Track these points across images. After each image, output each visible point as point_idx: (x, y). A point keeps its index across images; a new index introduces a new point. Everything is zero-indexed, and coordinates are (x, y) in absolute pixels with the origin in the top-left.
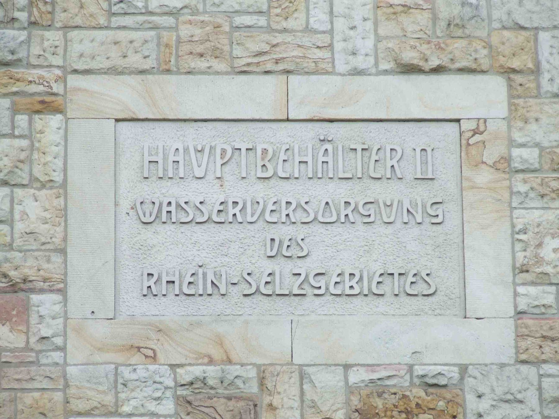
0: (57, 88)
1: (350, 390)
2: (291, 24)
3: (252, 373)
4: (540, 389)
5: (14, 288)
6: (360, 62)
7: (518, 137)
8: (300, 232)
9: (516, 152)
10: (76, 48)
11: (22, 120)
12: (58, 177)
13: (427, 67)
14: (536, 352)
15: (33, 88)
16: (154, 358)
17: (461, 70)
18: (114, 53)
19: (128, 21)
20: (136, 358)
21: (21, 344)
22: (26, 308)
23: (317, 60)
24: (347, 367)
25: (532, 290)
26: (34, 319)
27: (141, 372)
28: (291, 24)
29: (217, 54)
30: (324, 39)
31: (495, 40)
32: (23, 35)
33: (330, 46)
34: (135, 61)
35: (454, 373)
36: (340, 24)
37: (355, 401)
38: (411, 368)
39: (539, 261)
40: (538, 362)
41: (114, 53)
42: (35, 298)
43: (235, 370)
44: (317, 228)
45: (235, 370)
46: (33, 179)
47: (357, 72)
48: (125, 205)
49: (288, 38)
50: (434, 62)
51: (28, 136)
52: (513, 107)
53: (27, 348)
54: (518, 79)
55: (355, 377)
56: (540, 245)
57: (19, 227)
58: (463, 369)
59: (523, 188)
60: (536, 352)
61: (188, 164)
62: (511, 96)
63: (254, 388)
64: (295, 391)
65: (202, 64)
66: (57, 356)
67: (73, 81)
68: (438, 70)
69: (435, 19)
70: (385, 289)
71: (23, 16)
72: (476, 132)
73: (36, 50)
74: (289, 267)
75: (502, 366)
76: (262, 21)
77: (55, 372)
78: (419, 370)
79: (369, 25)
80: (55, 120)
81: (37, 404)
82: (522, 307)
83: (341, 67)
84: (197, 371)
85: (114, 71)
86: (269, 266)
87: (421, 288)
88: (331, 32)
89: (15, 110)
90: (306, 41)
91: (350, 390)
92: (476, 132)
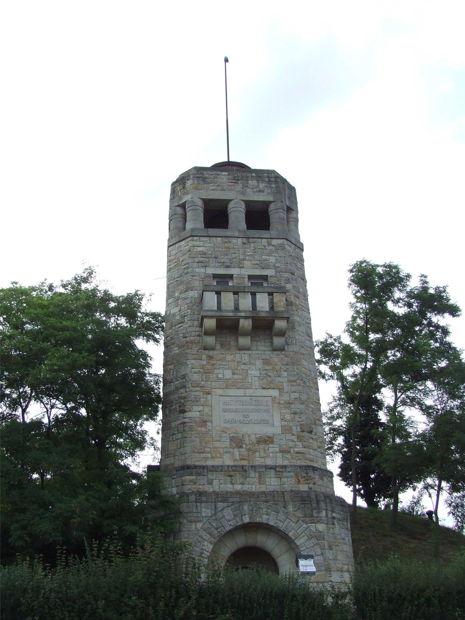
0: (210, 391)
1: (256, 438)
2: (246, 381)
3: (241, 435)
4: (285, 438)
5: (204, 422)
6: (257, 387)
7: (281, 399)
8: (248, 413)
9: (280, 401)
10: (213, 385)
11: (205, 396)
12: (211, 405)
13: (267, 388)
14: (284, 432)
15: (206, 391)
16: (226, 433)
17: (272, 389)
18: (219, 385)
19: (220, 380)
20: (223, 433)
21: (205, 430)
22: (206, 425)
23: (233, 387)
24: (256, 434)
25: (284, 422)
26: (207, 426)
27: (224, 435)
28: (246, 381)
29: (234, 386)
30: (250, 384)
31: (277, 384)
32: (205, 383)
33: (252, 385)
34: (222, 387)
35: (272, 435)
36: (253, 381)
37: (257, 440)
38: (266, 435)
39: (285, 418)
40: (285, 434)
41: (219, 385)
42: (207, 423)
43: (239, 435)
44: (250, 413)
45: (239, 435)
46: (207, 405)
47: (256, 389)
48: (221, 409)
49: (245, 383)
50: (268, 387)
51: (206, 398)
52: (280, 395)
53: (206, 431)
54: (281, 390)
55: (257, 436)
56: (285, 416)
57: (205, 412)
58: (274, 435)
59: (282, 407)
60: (284, 432)
61: (230, 403)
62: (279, 392)
63: (242, 438)
64: (248, 438)
65: (232, 387)
66: (211, 432)
67: (213, 390)
68: (268, 388)
69: (268, 381)
70: (261, 422)
71: (204, 380)
72: (275, 398)
73: (207, 385)
74: (246, 419)
75: (280, 434)
76: (241, 381)
77: (211, 435)
78: (267, 435)
79: (258, 382)
80: (210, 396)
81: (298, 398)
82: (282, 425)
83: (253, 388)
84: (233, 435)
85: (219, 388)
86: (244, 419)
87: (267, 422)
88: (252, 383)
89: (204, 394)
90: (248, 384)
91: (256, 438)
92: (275, 398)
